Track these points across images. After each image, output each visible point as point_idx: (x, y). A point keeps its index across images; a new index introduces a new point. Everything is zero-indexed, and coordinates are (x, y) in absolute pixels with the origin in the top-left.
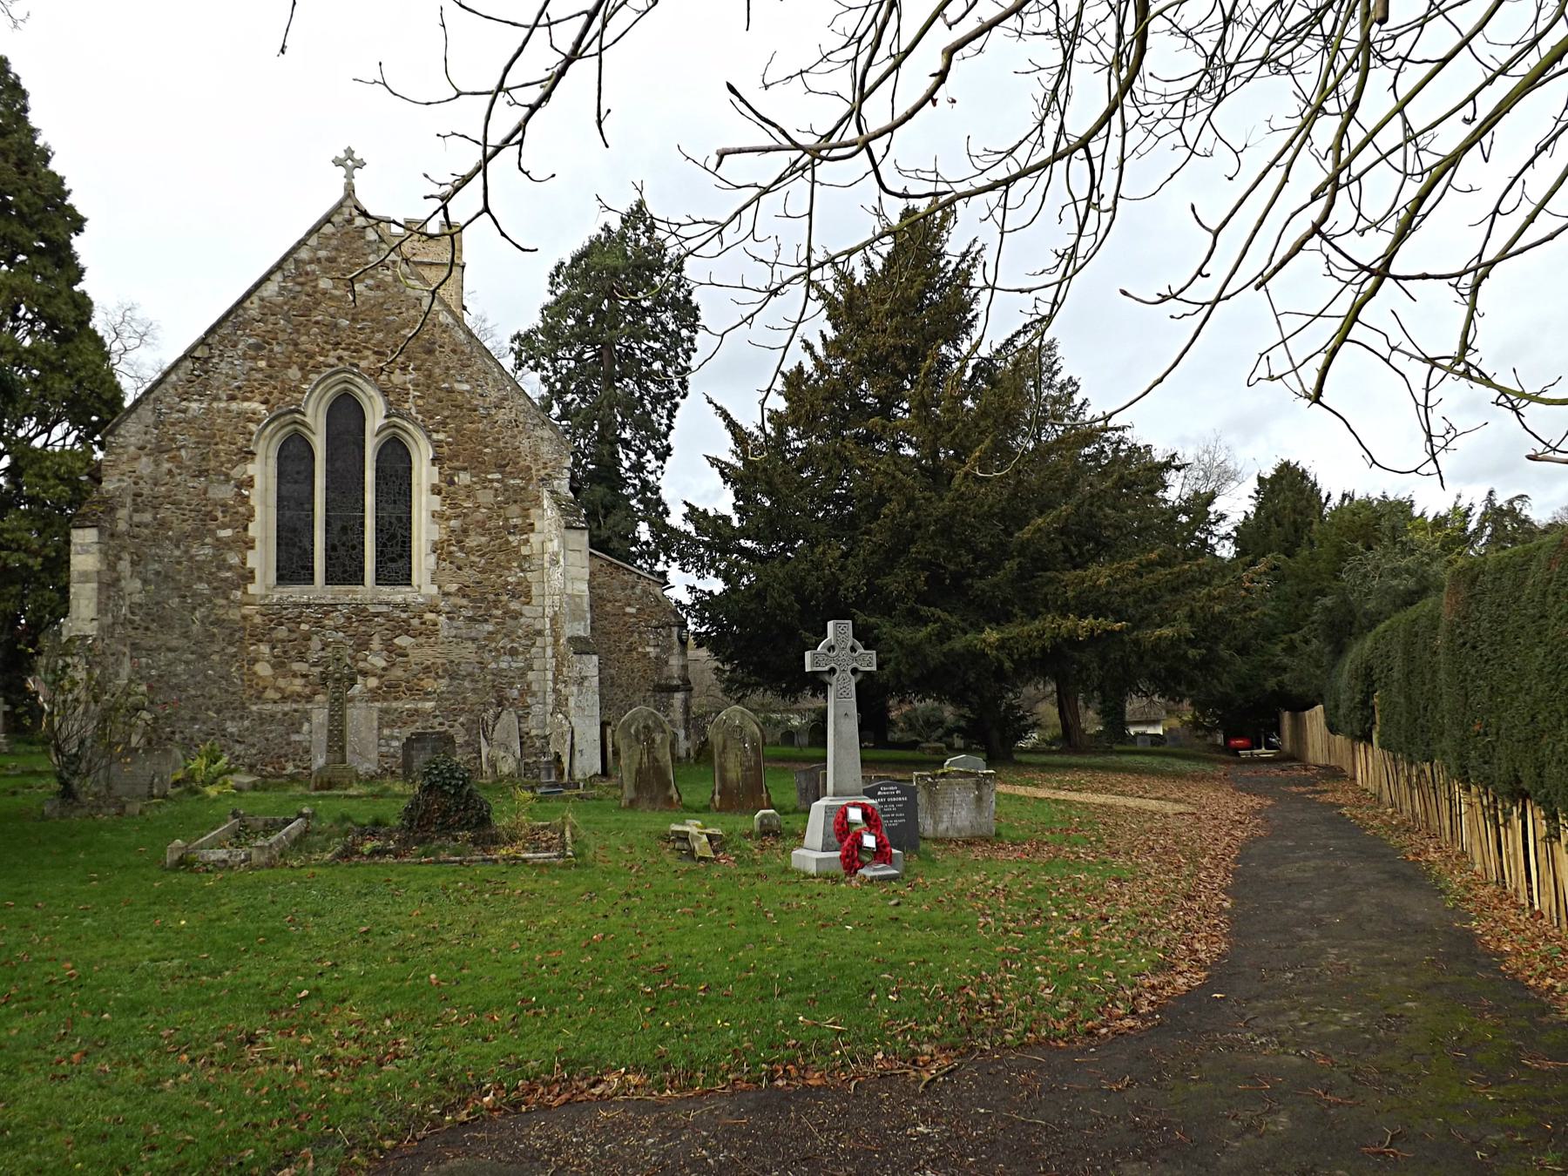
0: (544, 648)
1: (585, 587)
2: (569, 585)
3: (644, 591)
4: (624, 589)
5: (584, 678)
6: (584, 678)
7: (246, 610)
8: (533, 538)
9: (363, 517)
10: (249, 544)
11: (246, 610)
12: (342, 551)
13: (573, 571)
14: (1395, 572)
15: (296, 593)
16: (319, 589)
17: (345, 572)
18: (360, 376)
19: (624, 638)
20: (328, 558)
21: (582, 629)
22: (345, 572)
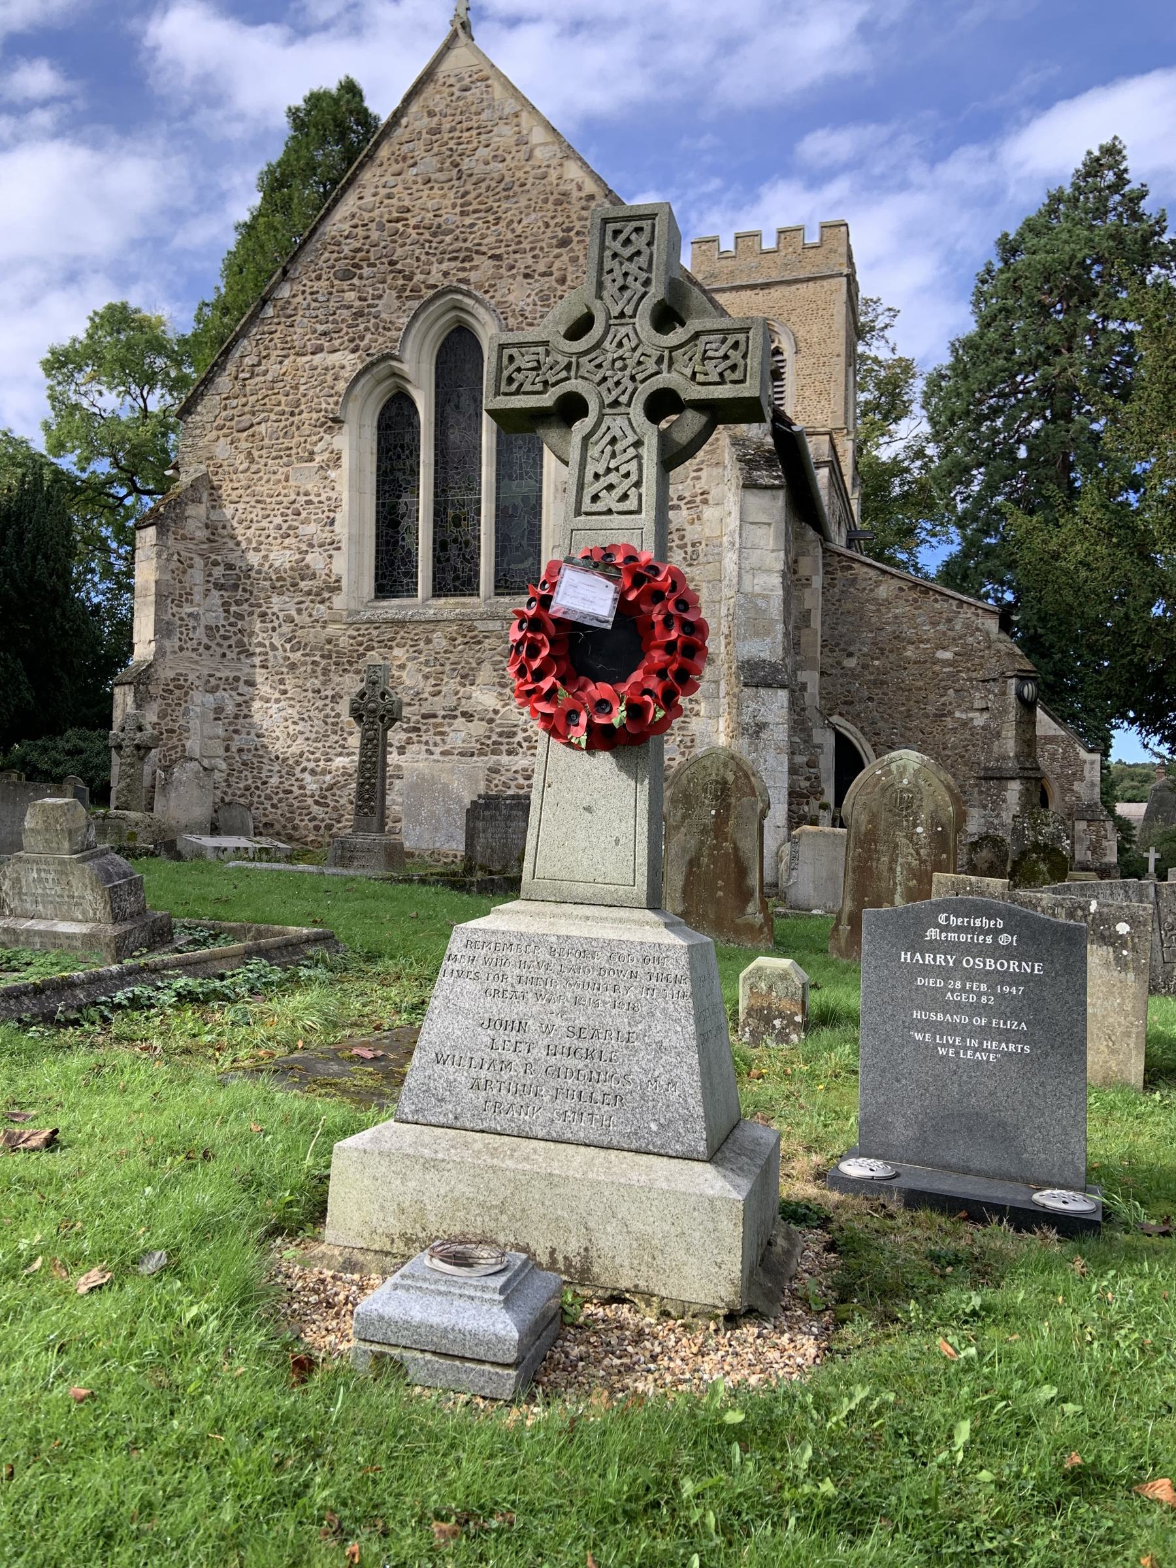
0: (717, 682)
1: (776, 581)
2: (747, 578)
3: (967, 626)
4: (934, 624)
5: (761, 727)
6: (761, 727)
7: (332, 629)
8: (709, 513)
9: (479, 501)
10: (334, 544)
11: (332, 629)
12: (453, 550)
13: (754, 557)
14: (119, 1159)
15: (393, 607)
16: (422, 602)
17: (457, 578)
18: (468, 294)
19: (932, 697)
20: (437, 560)
21: (768, 648)
22: (457, 578)
